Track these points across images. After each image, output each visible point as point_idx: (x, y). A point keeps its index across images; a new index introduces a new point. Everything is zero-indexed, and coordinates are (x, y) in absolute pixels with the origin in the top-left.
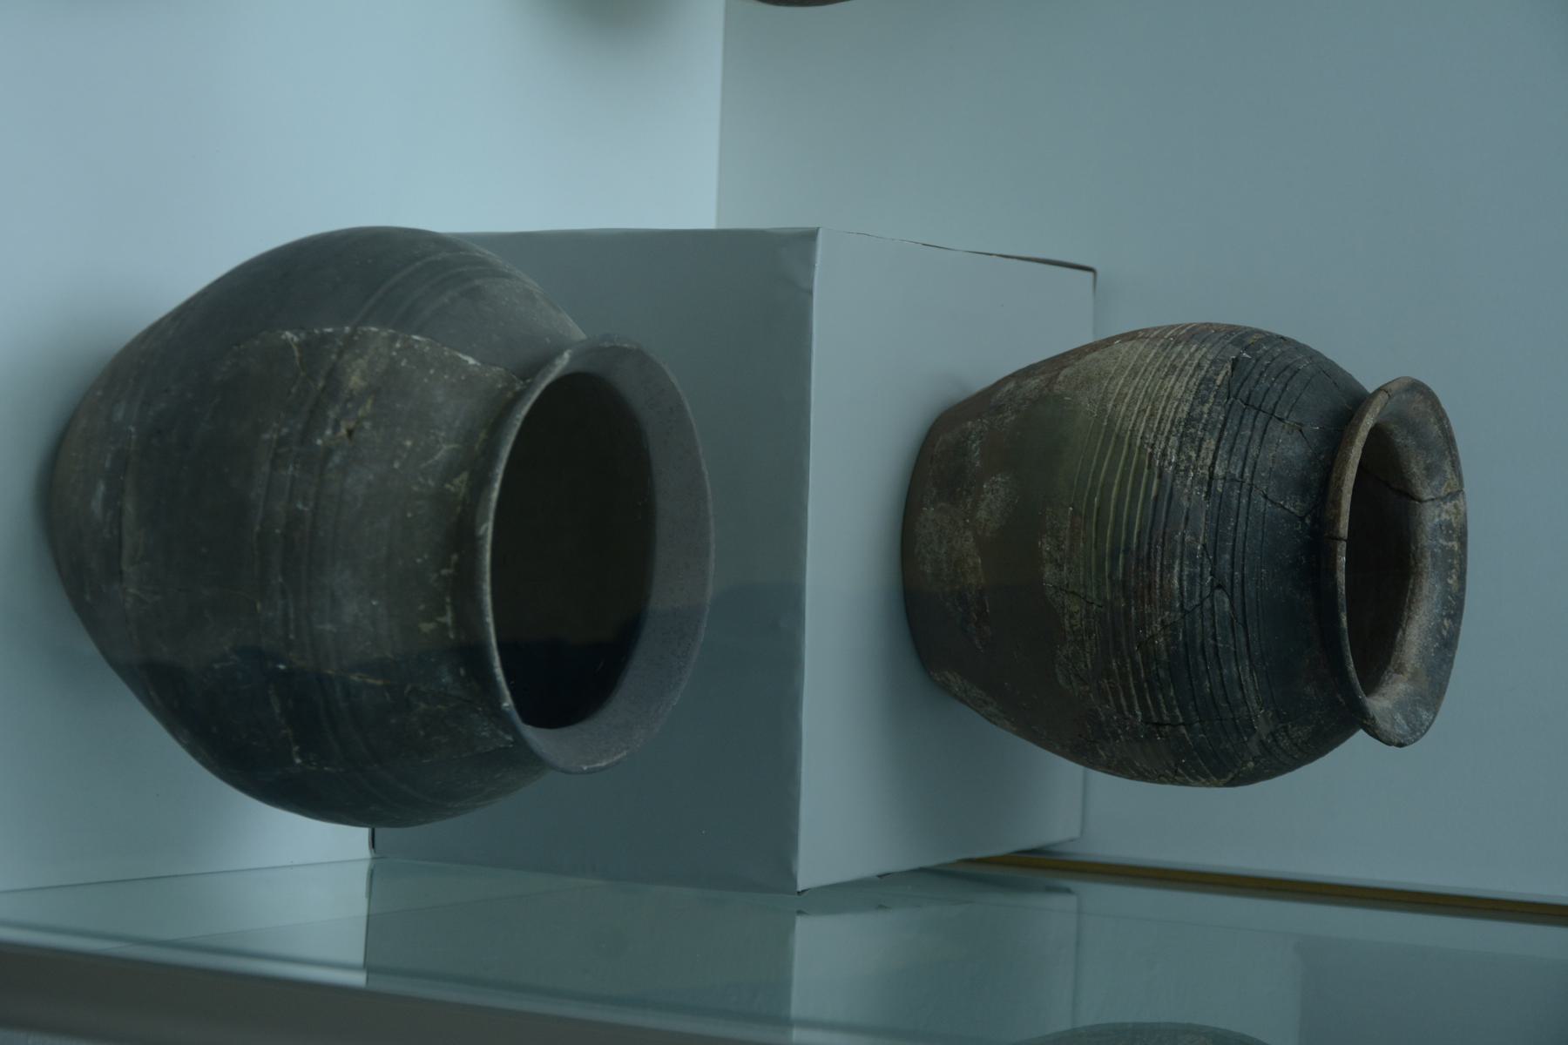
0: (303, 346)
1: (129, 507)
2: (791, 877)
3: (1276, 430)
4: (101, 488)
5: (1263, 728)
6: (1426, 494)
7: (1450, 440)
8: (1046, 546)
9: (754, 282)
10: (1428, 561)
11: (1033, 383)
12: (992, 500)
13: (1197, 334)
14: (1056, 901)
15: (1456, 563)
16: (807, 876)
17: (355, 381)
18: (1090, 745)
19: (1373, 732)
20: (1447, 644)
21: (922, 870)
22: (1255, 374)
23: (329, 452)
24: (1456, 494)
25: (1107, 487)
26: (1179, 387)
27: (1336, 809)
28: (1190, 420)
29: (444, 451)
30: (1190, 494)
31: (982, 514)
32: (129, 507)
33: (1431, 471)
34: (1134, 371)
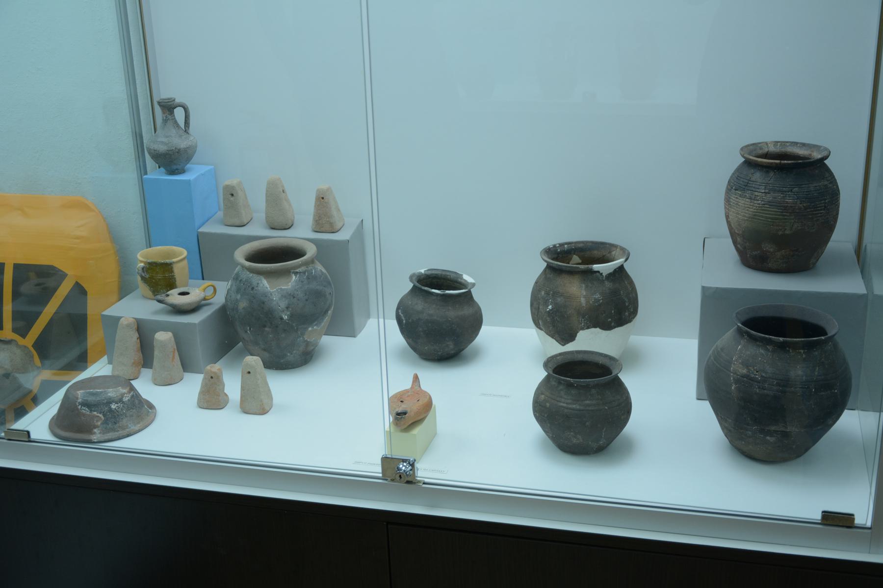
0: (736, 384)
1: (773, 428)
2: (864, 295)
3: (753, 179)
4: (768, 438)
5: (826, 183)
6: (766, 150)
7: (753, 144)
8: (780, 233)
9: (714, 301)
10: (783, 150)
11: (739, 239)
12: (769, 247)
13: (727, 200)
14: (868, 248)
15: (784, 143)
16: (865, 292)
17: (745, 371)
18: (829, 226)
19: (826, 158)
20: (804, 145)
21: (862, 272)
22: (738, 185)
23: (762, 376)
24: (767, 143)
25: (766, 218)
26: (742, 201)
27: (846, 170)
28: (751, 199)
29: (762, 351)
30: (769, 197)
31: (772, 250)
32: (773, 428)
33: (761, 149)
34: (738, 214)
